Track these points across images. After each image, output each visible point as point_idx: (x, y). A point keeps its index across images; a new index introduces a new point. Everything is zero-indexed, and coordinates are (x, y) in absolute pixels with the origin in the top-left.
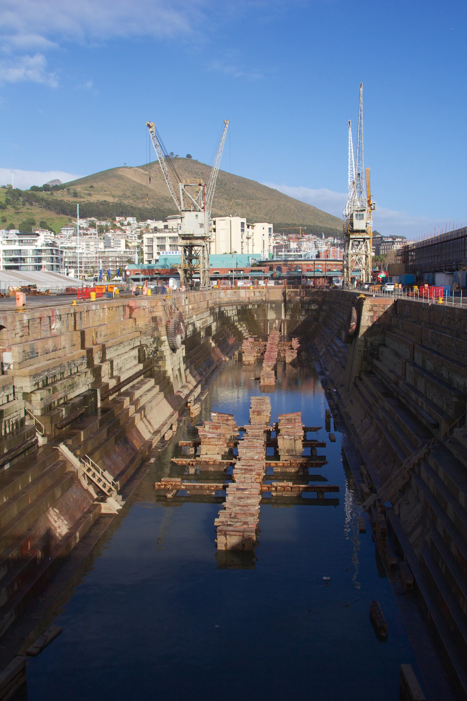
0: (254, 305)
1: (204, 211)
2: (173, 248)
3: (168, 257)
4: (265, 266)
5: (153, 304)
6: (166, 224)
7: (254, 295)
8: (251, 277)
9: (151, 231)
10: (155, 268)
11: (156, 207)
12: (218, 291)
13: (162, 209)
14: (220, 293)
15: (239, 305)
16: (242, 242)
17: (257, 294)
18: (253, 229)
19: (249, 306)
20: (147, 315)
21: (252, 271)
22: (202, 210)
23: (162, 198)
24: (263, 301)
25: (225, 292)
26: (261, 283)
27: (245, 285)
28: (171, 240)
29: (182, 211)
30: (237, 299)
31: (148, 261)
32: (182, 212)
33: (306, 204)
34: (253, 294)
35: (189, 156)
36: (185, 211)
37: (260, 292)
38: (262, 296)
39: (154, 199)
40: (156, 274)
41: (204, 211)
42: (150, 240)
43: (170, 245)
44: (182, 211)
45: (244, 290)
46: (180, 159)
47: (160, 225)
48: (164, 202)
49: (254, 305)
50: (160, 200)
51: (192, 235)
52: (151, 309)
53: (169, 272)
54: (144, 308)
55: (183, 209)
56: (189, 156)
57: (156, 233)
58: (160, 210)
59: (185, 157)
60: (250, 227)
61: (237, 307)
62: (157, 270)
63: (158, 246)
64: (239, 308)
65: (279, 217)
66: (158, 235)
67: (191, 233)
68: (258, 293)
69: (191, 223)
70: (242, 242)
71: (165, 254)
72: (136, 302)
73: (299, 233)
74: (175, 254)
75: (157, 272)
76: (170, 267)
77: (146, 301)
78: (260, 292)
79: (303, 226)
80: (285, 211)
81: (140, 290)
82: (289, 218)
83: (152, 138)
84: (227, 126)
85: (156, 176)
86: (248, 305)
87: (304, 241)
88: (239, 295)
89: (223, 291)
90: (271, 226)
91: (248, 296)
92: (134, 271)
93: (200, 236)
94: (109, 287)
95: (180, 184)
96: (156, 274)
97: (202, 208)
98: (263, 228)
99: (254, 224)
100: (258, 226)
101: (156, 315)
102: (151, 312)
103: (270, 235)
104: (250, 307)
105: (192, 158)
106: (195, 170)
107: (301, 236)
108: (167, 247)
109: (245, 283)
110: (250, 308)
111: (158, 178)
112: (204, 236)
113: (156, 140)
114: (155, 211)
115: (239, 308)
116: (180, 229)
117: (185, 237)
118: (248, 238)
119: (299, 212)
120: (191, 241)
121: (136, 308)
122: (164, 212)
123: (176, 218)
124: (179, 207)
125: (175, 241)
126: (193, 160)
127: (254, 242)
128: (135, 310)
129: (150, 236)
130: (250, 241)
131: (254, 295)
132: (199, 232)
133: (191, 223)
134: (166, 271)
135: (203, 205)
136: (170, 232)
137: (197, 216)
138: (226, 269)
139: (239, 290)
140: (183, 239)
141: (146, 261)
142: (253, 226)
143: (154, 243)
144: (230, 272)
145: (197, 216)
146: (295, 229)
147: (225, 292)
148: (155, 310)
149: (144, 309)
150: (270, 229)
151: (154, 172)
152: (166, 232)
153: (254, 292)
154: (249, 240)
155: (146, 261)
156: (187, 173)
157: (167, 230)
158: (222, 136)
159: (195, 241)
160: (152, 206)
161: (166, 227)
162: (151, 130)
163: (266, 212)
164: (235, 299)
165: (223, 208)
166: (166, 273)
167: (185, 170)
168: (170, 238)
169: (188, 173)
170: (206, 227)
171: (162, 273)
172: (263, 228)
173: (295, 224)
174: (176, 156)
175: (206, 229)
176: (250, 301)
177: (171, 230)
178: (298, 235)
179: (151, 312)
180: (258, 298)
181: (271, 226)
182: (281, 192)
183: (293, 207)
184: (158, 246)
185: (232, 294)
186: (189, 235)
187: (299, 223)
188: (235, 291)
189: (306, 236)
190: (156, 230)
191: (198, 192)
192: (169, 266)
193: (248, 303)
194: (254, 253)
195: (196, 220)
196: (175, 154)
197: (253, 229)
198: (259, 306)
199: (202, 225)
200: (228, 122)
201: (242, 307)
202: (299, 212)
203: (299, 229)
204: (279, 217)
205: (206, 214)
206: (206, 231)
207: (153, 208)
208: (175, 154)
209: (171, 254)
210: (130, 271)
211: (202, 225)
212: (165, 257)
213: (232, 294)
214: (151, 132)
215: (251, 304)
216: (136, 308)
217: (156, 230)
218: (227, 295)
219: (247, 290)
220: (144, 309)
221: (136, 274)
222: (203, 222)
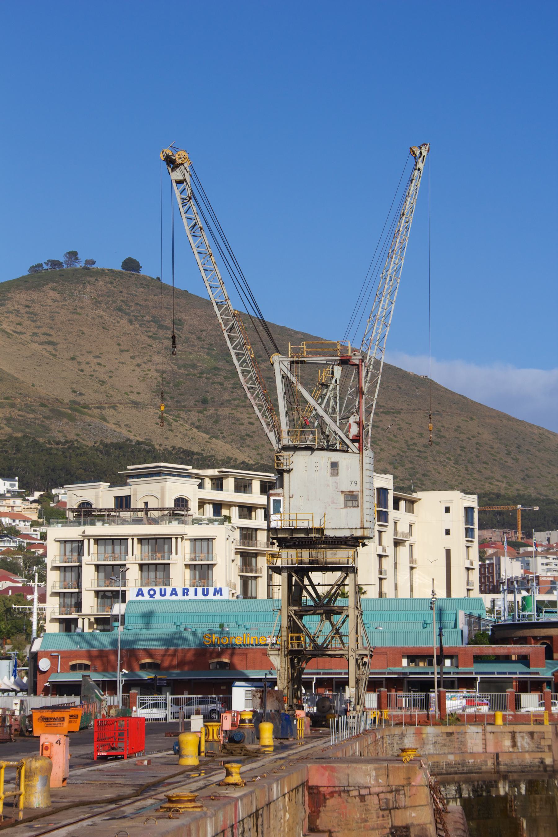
0: (515, 784)
1: (360, 449)
2: (152, 574)
3: (158, 609)
4: (524, 640)
5: (397, 780)
6: (122, 491)
7: (514, 745)
8: (483, 681)
9: (70, 516)
10: (139, 646)
11: (19, 435)
12: (397, 731)
13: (41, 440)
14: (402, 736)
15: (466, 781)
16: (380, 556)
17: (524, 742)
18: (410, 510)
19: (500, 785)
20: (374, 820)
21: (479, 659)
22: (354, 447)
23: (42, 405)
24: (546, 767)
25: (419, 733)
26: (530, 703)
27: (471, 710)
28: (146, 548)
29: (286, 448)
30: (458, 759)
31: (61, 621)
32: (284, 453)
33: (531, 426)
34: (507, 743)
35: (131, 265)
36: (295, 449)
37: (532, 734)
38: (539, 749)
39: (13, 406)
40: (143, 667)
41: (360, 449)
42: (68, 546)
43: (141, 566)
44: (286, 448)
45: (479, 729)
46: (102, 273)
47: (102, 495)
48: (48, 418)
49: (515, 784)
50: (34, 411)
51: (320, 530)
52: (390, 796)
53: (190, 662)
54: (363, 792)
55: (285, 441)
56: (131, 265)
57: (93, 523)
58: (36, 444)
59: (118, 267)
60: (402, 504)
61: (459, 791)
62: (149, 653)
63: (98, 567)
64: (465, 795)
65: (440, 469)
66: (100, 529)
67: (317, 525)
68: (527, 739)
69: (319, 489)
70: (380, 556)
71: (147, 597)
72: (333, 770)
73: (513, 526)
74: (200, 596)
75: (148, 661)
76: (192, 642)
77: (370, 767)
78: (532, 734)
79: (527, 501)
80: (463, 449)
81: (247, 725)
82: (476, 476)
83: (179, 201)
84: (420, 165)
85: (20, 329)
86: (496, 782)
87: (537, 554)
88: (463, 743)
89: (411, 730)
90: (472, 501)
91: (491, 749)
92: (67, 655)
93: (347, 534)
94: (36, 716)
95: (276, 357)
96: (143, 667)
97: (353, 441)
98: (447, 510)
99: (414, 495)
100: (430, 501)
101: (409, 822)
102: (389, 809)
103: (469, 532)
104: (503, 789)
105: (143, 272)
106: (154, 312)
107: (520, 535)
108: (133, 574)
109: (470, 702)
110: (502, 793)
111: (27, 337)
112: (358, 533)
113: (195, 209)
114: (18, 450)
115: (465, 795)
116: (277, 511)
117: (288, 539)
118: (397, 543)
119: (509, 454)
120: (314, 552)
121: (332, 794)
122: (49, 451)
123: (158, 474)
124: (272, 436)
125: (161, 551)
126: (144, 278)
127: (415, 557)
128: (330, 802)
129: (73, 533)
130: (403, 551)
131: (514, 745)
132: (340, 521)
133: (319, 489)
134: (179, 654)
135: (354, 430)
136: (137, 521)
137: (334, 465)
138: (394, 650)
139: (461, 729)
140: (284, 543)
141: (53, 620)
142: (411, 502)
143: (85, 559)
144: (405, 662)
145: (334, 465)
146: (500, 513)
147: (419, 733)
148: (402, 800)
149: (362, 798)
150: (469, 510)
151: (12, 317)
152: (124, 522)
153: (513, 735)
154: (400, 549)
155: (53, 620)
156: (124, 322)
157: (124, 515)
158: (405, 198)
159: (329, 552)
160: (8, 430)
161: (123, 503)
162: (177, 175)
163: (395, 452)
164: (451, 758)
165: (248, 441)
166: (180, 665)
167: (120, 309)
168: (140, 541)
169: (130, 322)
170: (366, 505)
171: (166, 664)
172: (447, 510)
173: (498, 496)
174: (87, 262)
175: (367, 511)
176: (502, 768)
177: (141, 515)
178: (512, 532)
179: (389, 809)
180: (528, 758)
181: (472, 501)
182: (438, 382)
183: (486, 436)
184: (98, 567)
185: (440, 739)
186: (307, 531)
187: (512, 492)
188: (449, 729)
189: (539, 537)
190: (86, 513)
191: (325, 386)
192: (191, 638)
193: (494, 777)
194: (416, 595)
195: (331, 480)
196: (83, 257)
197: (410, 510)
198: (532, 786)
199: (351, 498)
200: (425, 153)
201: (475, 791)
202: (509, 454)
203: (515, 511)
204: (440, 469)
205: (366, 460)
206: (367, 518)
207: (11, 437)
208: (83, 257)
209: (168, 597)
210: (52, 657)
211: (351, 498)
212: (146, 608)
213: (440, 739)
214: (179, 182)
215: (505, 777)
216: (332, 794)
217: (86, 513)
218: (423, 743)
219: (489, 728)
220: (362, 798)
221: (74, 668)
222: (356, 488)
